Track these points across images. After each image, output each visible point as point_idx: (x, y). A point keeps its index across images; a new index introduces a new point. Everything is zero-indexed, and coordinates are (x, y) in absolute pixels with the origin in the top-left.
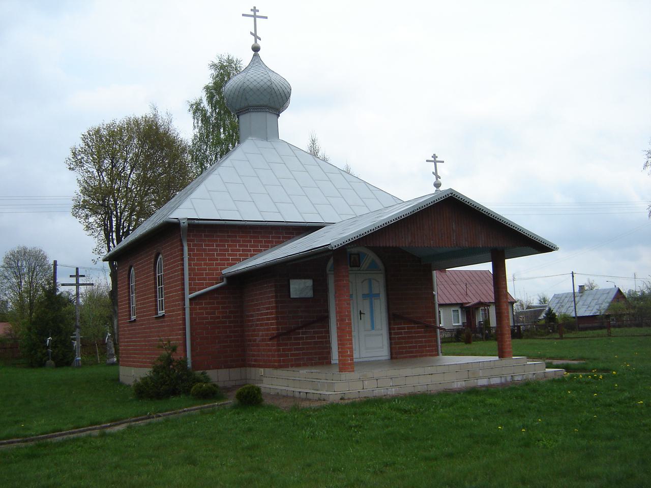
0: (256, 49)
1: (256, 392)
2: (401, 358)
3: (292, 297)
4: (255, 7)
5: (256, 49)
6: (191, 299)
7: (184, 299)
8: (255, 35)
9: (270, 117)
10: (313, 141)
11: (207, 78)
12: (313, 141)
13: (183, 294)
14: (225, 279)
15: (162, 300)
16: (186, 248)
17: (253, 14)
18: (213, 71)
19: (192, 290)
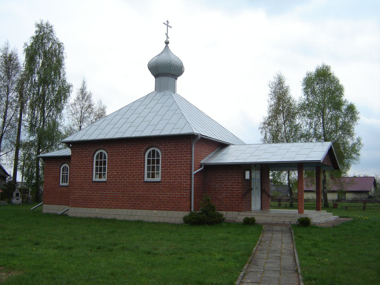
0: (167, 43)
1: (250, 221)
2: (232, 221)
3: (246, 178)
4: (168, 20)
5: (167, 43)
6: (195, 175)
7: (191, 175)
8: (167, 35)
9: (171, 79)
10: (84, 82)
11: (32, 32)
12: (84, 82)
13: (191, 172)
14: (203, 166)
15: (65, 175)
16: (193, 149)
17: (167, 24)
18: (37, 29)
19: (195, 170)
